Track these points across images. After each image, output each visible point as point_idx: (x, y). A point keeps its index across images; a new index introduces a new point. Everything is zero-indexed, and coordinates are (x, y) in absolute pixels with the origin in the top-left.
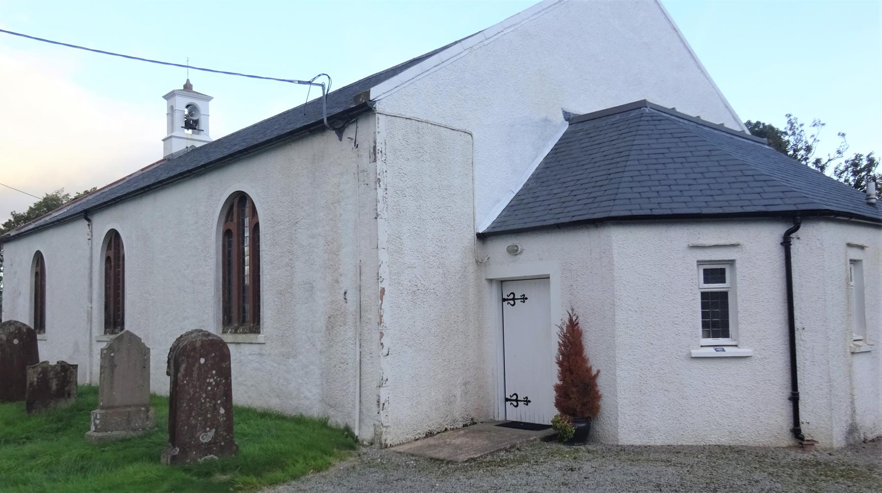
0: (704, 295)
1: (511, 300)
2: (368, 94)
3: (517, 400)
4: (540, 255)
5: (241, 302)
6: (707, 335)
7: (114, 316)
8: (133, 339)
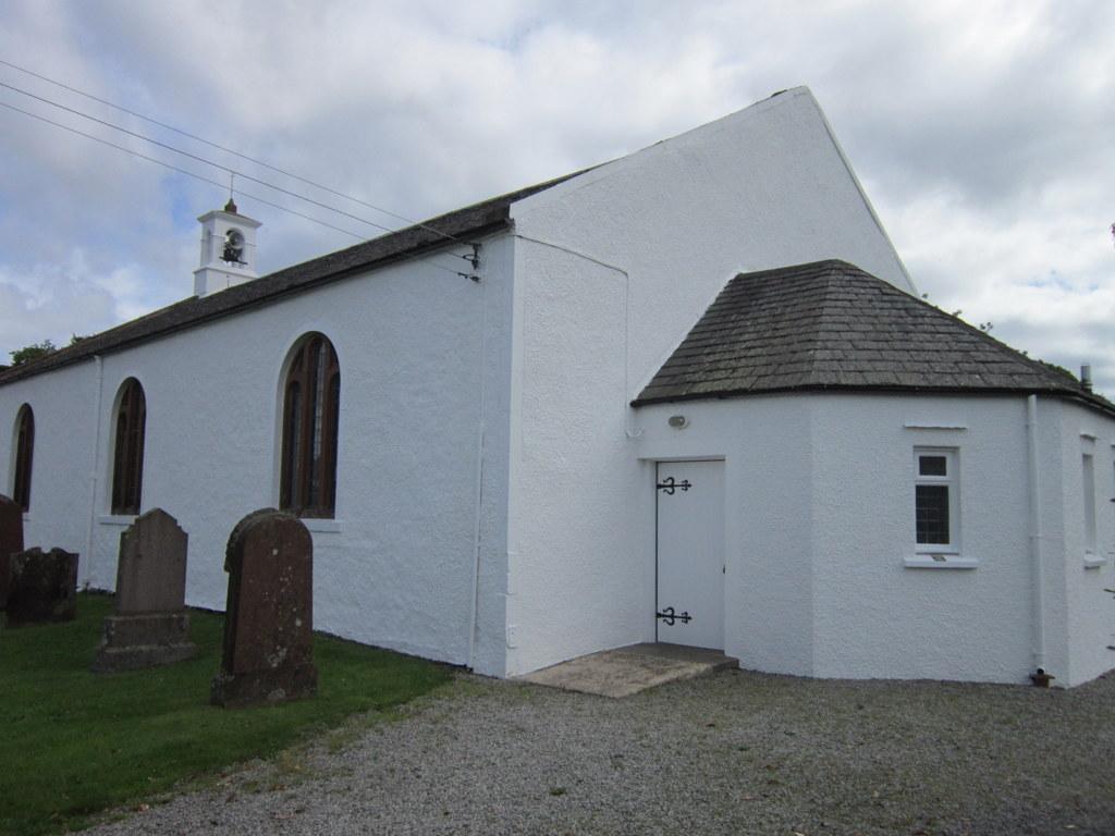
0: (920, 490)
1: (666, 486)
2: (507, 210)
3: (672, 617)
4: (711, 427)
5: (310, 474)
6: (921, 539)
7: (126, 491)
8: (161, 517)
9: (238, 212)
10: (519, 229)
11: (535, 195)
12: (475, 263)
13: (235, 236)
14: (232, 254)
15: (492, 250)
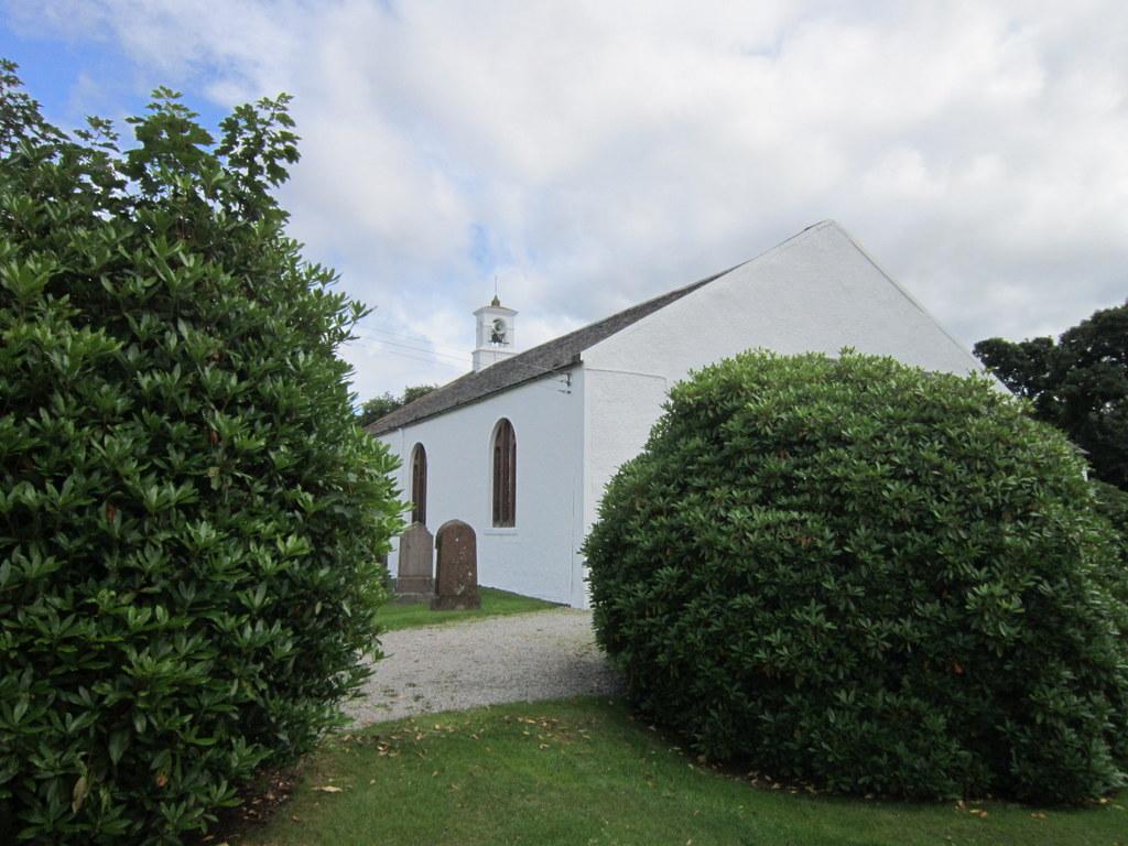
9: (501, 305)
10: (586, 365)
11: (641, 322)
12: (569, 384)
13: (499, 324)
14: (496, 338)
15: (576, 373)
